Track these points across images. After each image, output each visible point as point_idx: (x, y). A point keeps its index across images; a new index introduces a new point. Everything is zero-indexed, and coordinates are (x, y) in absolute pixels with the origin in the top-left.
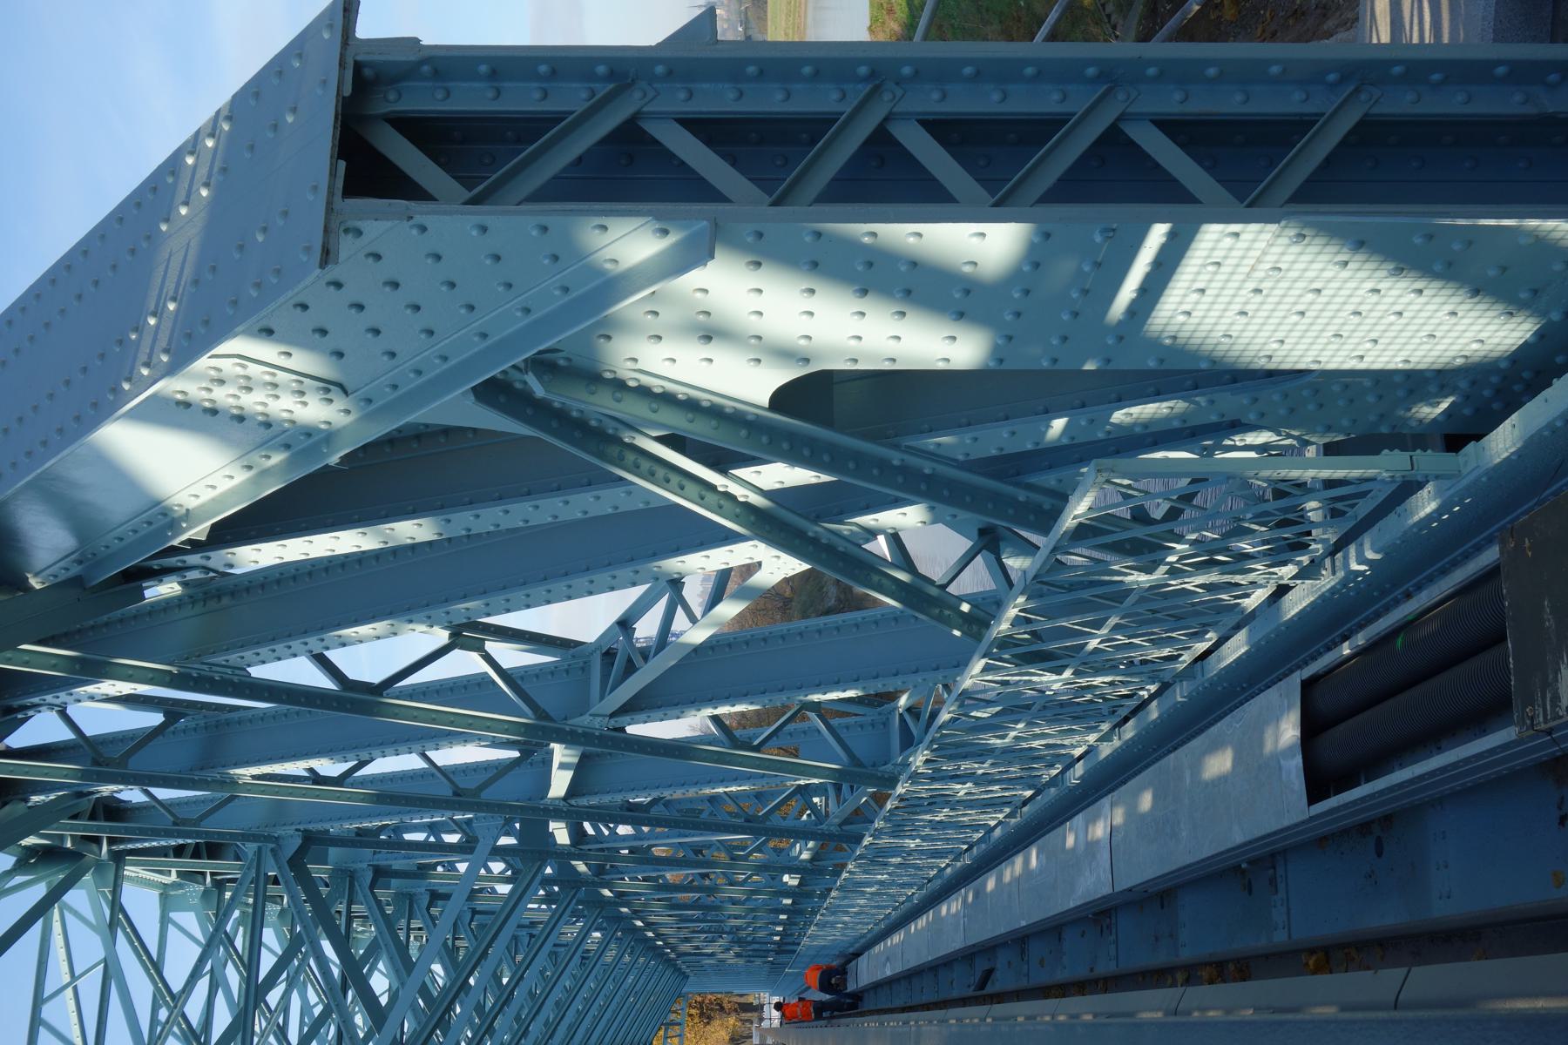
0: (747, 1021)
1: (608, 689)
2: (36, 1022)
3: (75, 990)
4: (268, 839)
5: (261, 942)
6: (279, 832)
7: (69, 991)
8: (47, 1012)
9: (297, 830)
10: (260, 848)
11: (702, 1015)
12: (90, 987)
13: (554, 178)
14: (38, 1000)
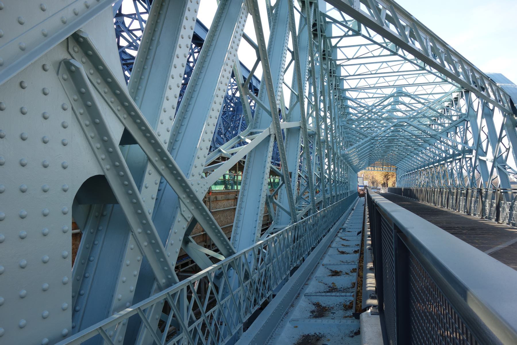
4: (468, 116)
6: (469, 117)
11: (386, 175)
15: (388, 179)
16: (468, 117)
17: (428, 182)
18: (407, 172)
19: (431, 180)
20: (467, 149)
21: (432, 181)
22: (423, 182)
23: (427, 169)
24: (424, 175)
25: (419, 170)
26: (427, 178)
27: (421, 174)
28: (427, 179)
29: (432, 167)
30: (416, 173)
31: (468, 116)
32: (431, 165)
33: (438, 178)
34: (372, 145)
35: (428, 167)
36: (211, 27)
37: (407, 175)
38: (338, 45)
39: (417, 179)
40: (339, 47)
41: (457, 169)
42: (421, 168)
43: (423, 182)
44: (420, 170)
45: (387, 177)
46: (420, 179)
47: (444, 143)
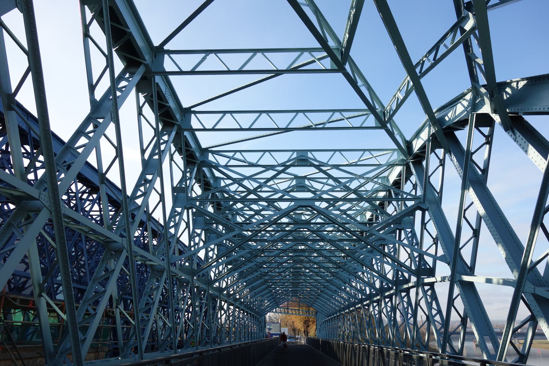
0: (299, 334)
1: (111, 240)
2: (365, 150)
3: (372, 158)
4: (424, 200)
5: (322, 201)
6: (426, 203)
7: (372, 156)
8: (367, 153)
9: (428, 207)
10: (420, 198)
11: (306, 321)
12: (373, 161)
13: (33, 221)
14: (369, 150)
15: (308, 326)
16: (424, 202)
17: (354, 332)
18: (328, 317)
19: (358, 328)
20: (401, 278)
21: (360, 330)
22: (347, 332)
23: (353, 311)
24: (349, 320)
25: (341, 313)
26: (354, 325)
27: (344, 319)
28: (354, 327)
29: (359, 308)
30: (338, 317)
31: (424, 200)
32: (358, 304)
33: (370, 326)
34: (267, 278)
35: (353, 308)
36: (68, 141)
37: (327, 320)
38: (166, 47)
39: (340, 327)
40: (169, 52)
41: (387, 312)
42: (344, 309)
43: (347, 332)
44: (343, 312)
45: (306, 323)
46: (343, 327)
47: (359, 279)
